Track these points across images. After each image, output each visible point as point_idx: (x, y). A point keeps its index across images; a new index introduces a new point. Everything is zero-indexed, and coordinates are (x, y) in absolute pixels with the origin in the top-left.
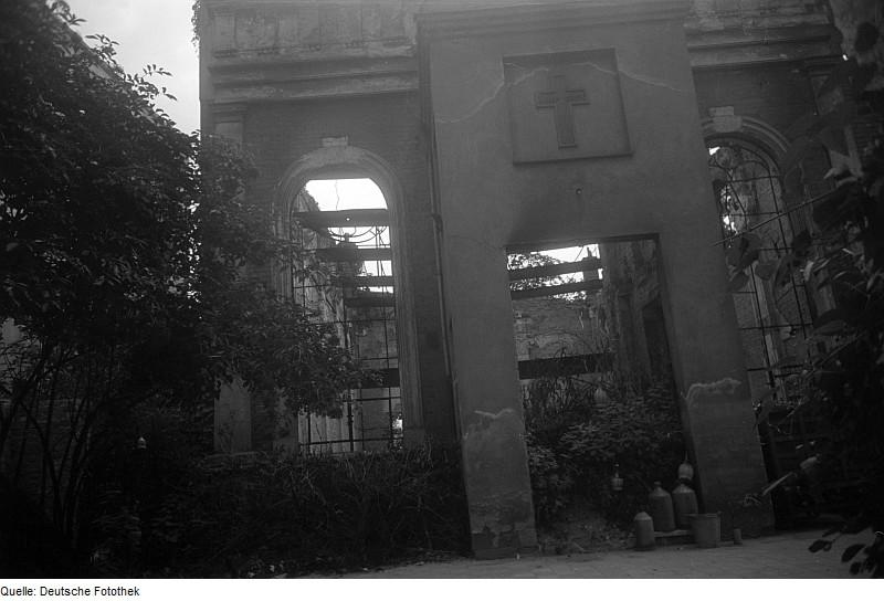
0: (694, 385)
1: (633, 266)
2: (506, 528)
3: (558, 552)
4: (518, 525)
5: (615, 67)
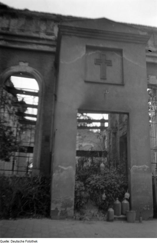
2: (64, 209)
3: (80, 219)
4: (68, 209)
5: (122, 55)
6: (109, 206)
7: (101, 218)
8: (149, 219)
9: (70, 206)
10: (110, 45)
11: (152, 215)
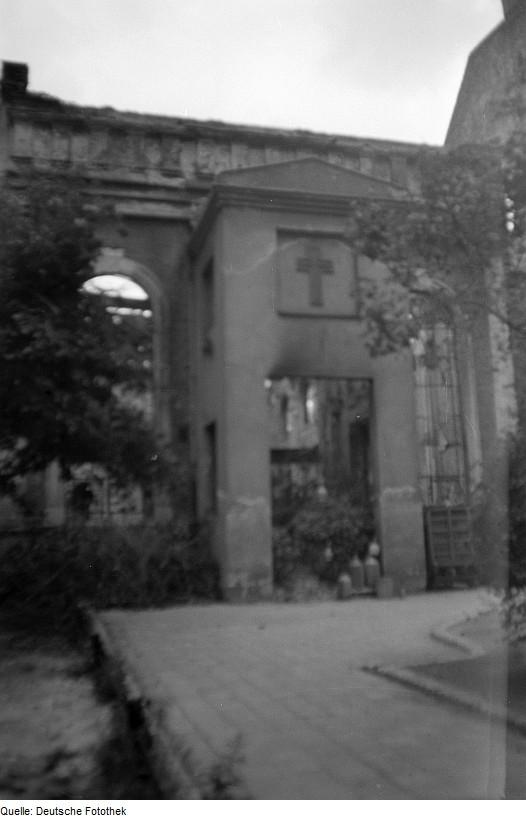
4: (261, 582)
6: (340, 571)
8: (418, 591)
11: (423, 583)
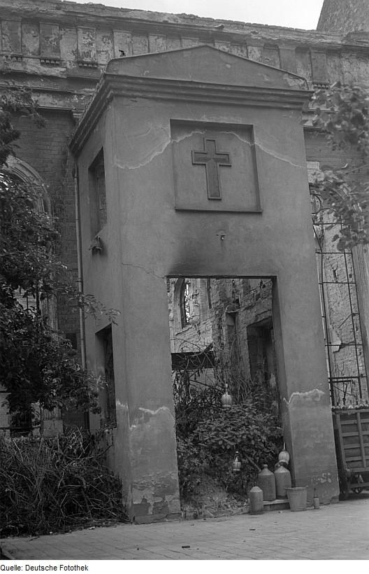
0: (294, 393)
1: (242, 291)
2: (160, 500)
3: (196, 517)
4: (168, 498)
5: (252, 140)
7: (236, 510)
8: (331, 501)
9: (171, 492)
10: (226, 118)
11: (337, 493)
